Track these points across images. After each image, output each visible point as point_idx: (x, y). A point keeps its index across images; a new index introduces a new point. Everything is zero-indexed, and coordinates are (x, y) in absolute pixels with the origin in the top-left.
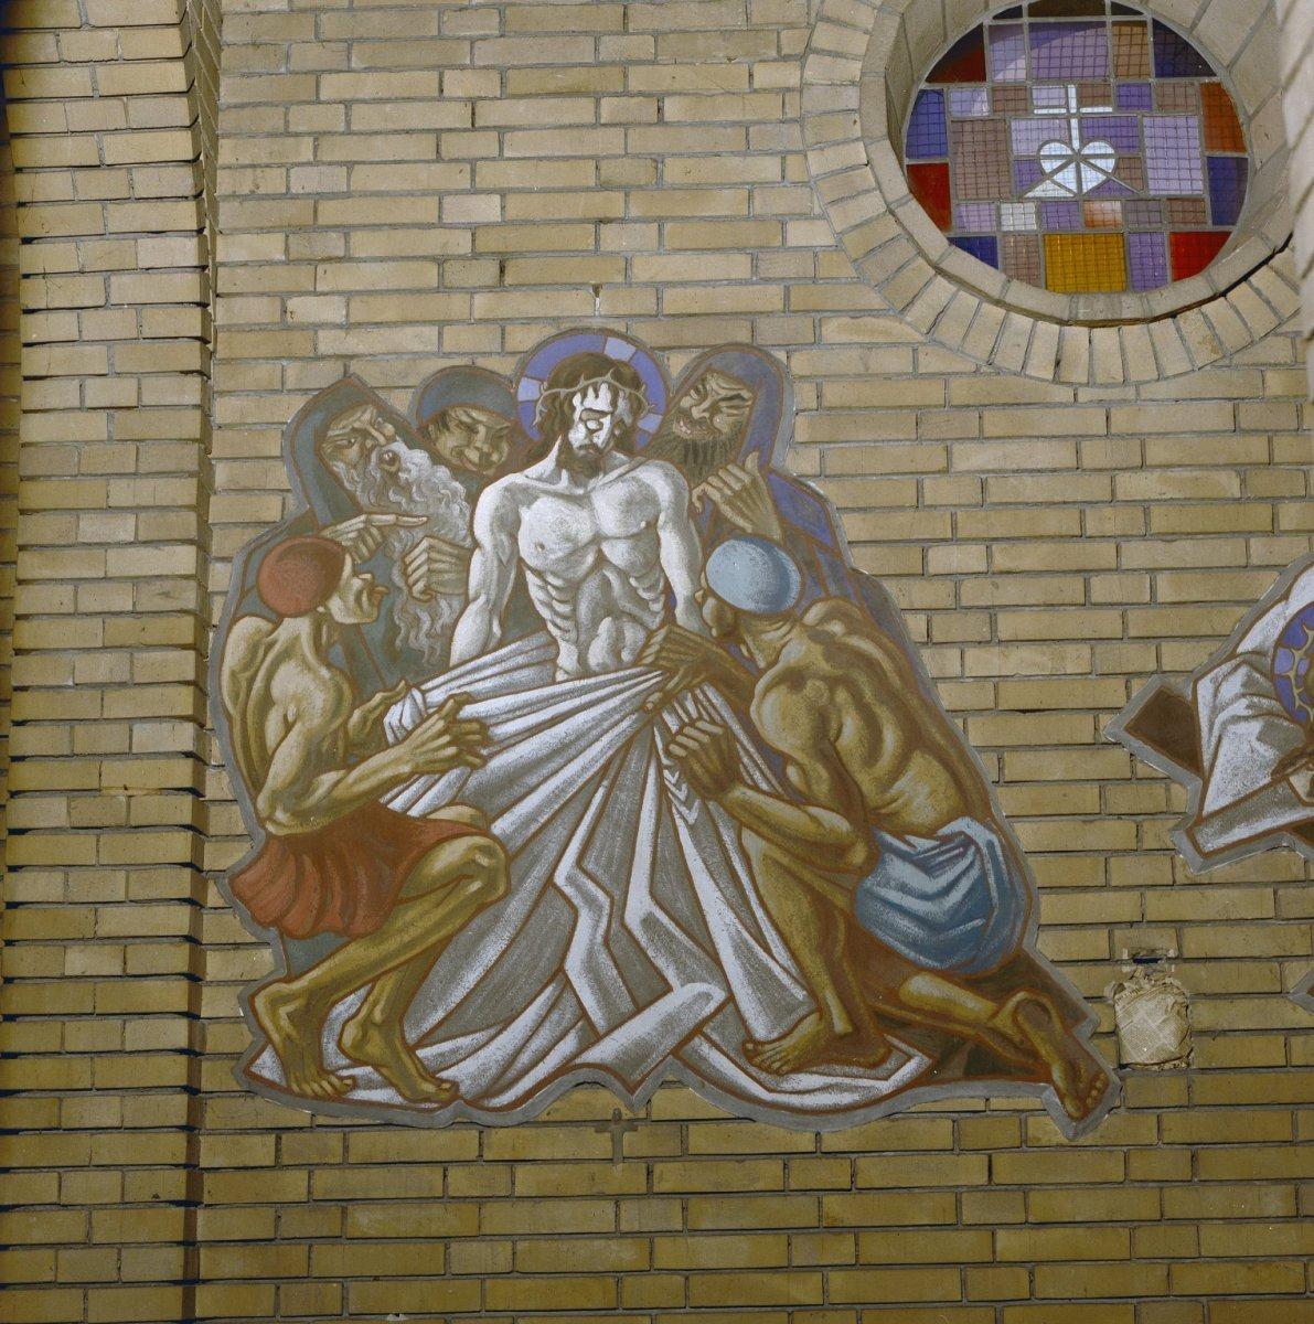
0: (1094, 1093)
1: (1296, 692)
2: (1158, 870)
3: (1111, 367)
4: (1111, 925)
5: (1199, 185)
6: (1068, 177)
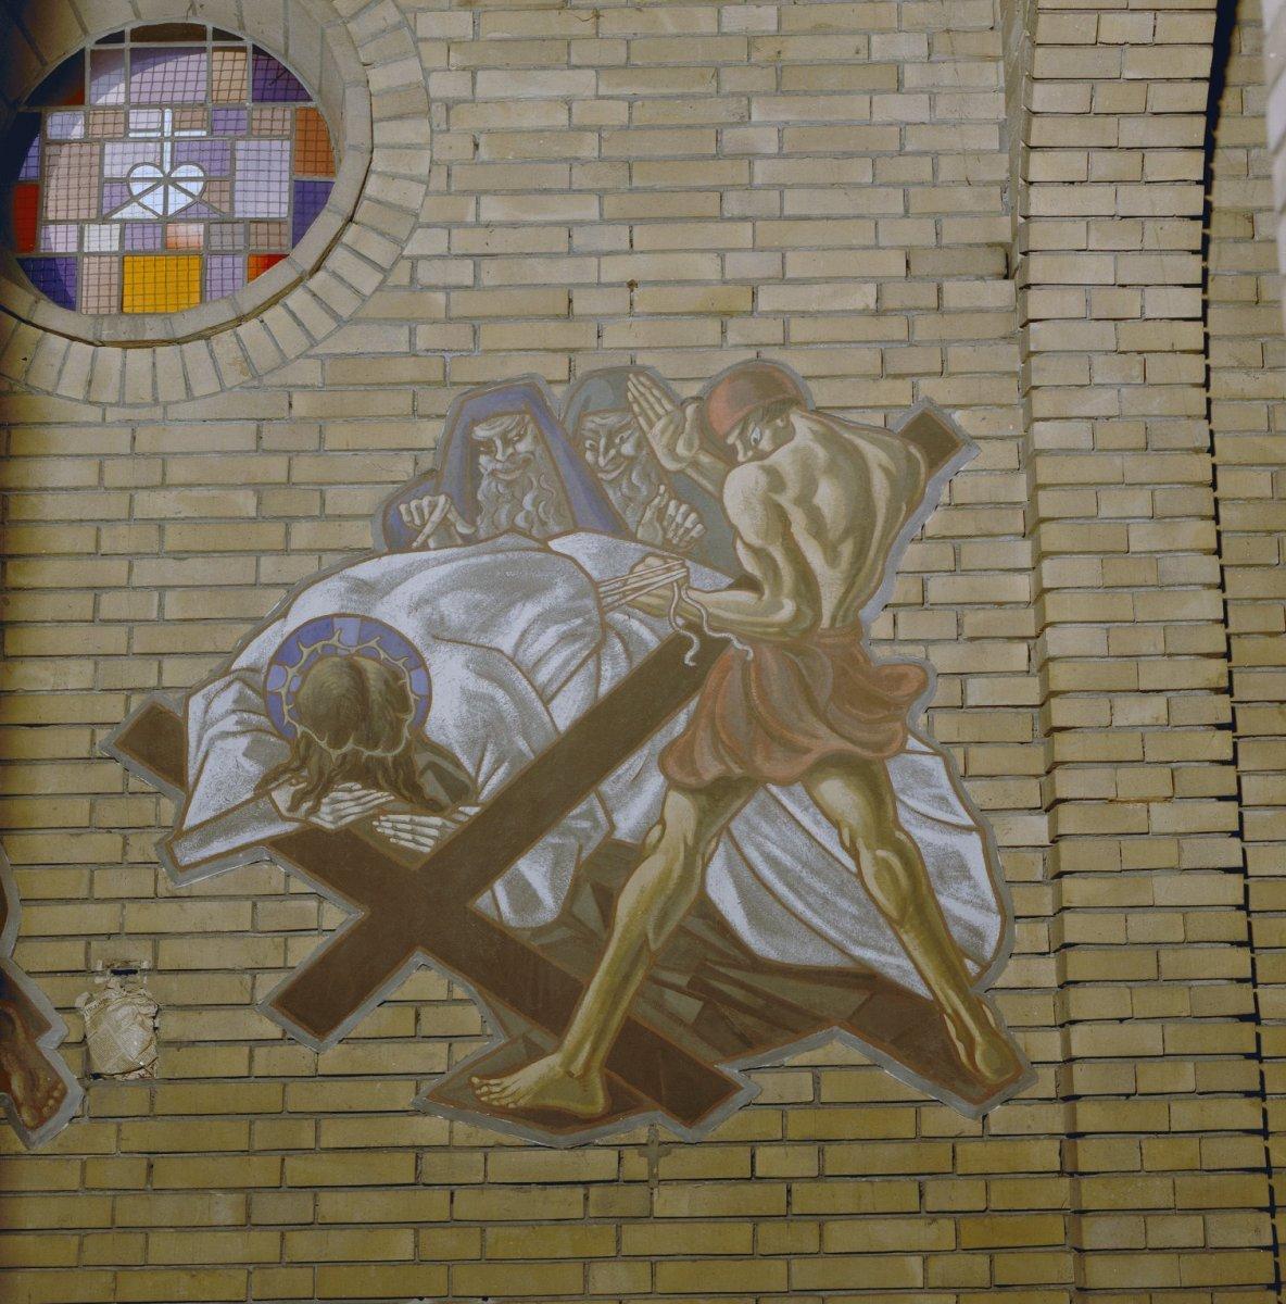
0: (51, 1102)
1: (286, 708)
2: (141, 882)
3: (140, 388)
4: (89, 936)
5: (285, 208)
6: (154, 200)
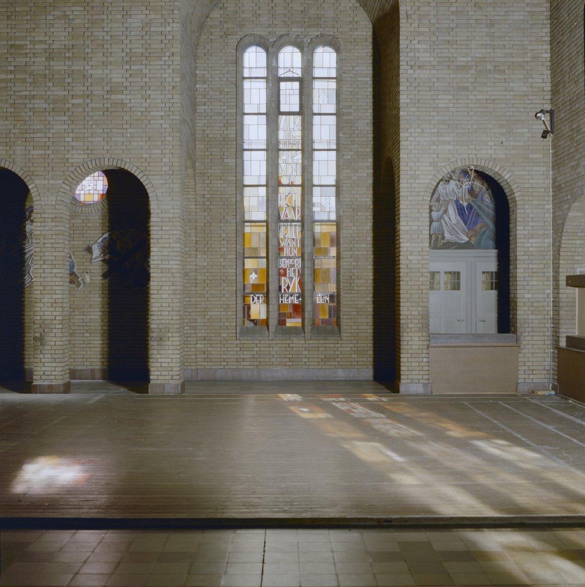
6: (88, 188)
